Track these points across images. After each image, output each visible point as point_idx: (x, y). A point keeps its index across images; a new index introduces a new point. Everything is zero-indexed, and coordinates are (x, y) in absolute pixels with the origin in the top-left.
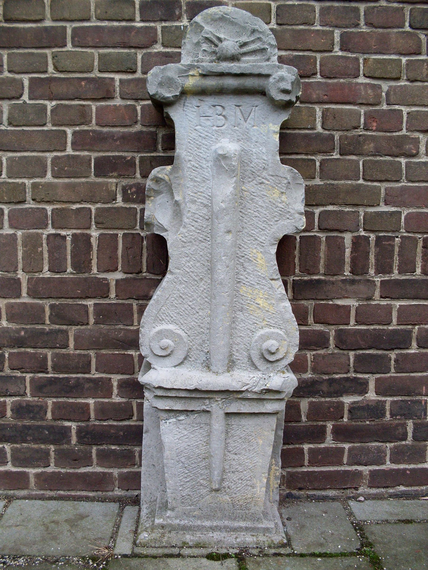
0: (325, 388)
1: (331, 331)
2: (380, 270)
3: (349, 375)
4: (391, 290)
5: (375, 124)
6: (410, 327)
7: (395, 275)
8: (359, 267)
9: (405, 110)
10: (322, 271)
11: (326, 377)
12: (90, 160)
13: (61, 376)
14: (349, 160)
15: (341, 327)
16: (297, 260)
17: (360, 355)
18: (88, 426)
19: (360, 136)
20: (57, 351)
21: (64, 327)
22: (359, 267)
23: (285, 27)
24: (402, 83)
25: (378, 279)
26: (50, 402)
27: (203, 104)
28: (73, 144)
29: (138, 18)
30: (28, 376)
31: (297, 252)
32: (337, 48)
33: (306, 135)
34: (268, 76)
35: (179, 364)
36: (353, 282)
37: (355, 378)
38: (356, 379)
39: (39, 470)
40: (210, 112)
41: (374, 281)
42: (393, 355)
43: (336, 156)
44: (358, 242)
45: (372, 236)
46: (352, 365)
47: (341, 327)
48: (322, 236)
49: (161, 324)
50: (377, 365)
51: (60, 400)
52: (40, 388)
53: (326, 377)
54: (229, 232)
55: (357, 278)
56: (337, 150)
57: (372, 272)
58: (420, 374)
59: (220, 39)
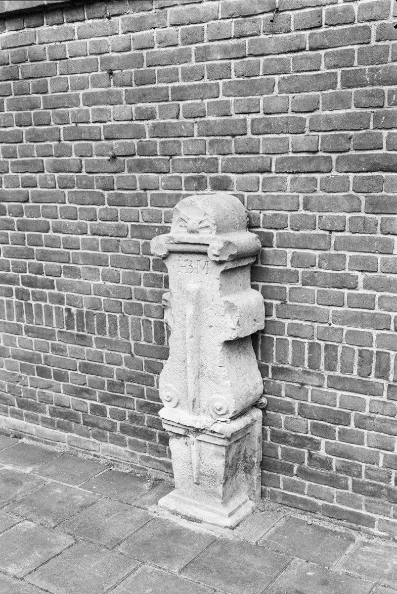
0: (291, 440)
1: (296, 404)
2: (329, 367)
3: (307, 435)
4: (335, 383)
5: (325, 264)
6: (350, 411)
7: (338, 373)
8: (313, 365)
9: (348, 254)
10: (290, 363)
11: (294, 433)
12: (162, 277)
13: (151, 402)
14: (308, 289)
15: (303, 402)
16: (274, 353)
17: (314, 423)
18: (163, 433)
19: (316, 272)
20: (149, 387)
21: (152, 374)
22: (313, 365)
23: (267, 193)
24: (347, 234)
25: (326, 374)
26: (146, 415)
27: (181, 259)
28: (153, 267)
29: (184, 189)
30: (136, 399)
31: (274, 349)
32: (301, 208)
33: (279, 270)
34: (208, 245)
35: (175, 407)
36: (308, 373)
37: (312, 438)
38: (311, 439)
39: (142, 454)
40: (184, 264)
41: (323, 375)
42: (337, 428)
43: (299, 285)
44: (312, 346)
45: (322, 344)
46: (309, 429)
47: (303, 402)
48: (290, 339)
49: (168, 384)
50: (327, 433)
51: (151, 416)
52: (142, 406)
53: (294, 433)
54: (192, 337)
55: (312, 371)
56: (300, 282)
57: (322, 367)
58: (357, 446)
59: (189, 219)
